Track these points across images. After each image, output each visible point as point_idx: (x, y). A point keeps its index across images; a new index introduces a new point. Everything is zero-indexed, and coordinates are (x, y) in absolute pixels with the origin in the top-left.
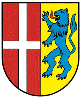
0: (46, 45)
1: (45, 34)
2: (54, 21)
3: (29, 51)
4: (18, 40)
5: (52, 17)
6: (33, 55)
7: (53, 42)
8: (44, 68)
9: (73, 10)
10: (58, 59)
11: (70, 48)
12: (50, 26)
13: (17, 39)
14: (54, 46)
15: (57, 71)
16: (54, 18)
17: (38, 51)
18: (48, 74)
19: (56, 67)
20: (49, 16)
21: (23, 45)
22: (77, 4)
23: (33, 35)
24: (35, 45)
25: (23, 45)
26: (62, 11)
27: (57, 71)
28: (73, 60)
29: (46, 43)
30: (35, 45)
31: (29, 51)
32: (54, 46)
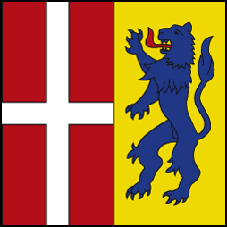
0: (137, 116)
1: (129, 78)
2: (156, 54)
3: (76, 132)
4: (71, 127)
5: (150, 43)
6: (91, 146)
7: (155, 107)
8: (126, 172)
9: (206, 22)
10: (166, 152)
11: (199, 125)
12: (146, 63)
13: (41, 96)
14: (156, 116)
15: (173, 181)
16: (157, 46)
17: (107, 132)
18: (141, 189)
19: (161, 172)
20: (143, 42)
21: (57, 113)
22: (112, 123)
23: (91, 80)
24: (95, 113)
25: (57, 113)
26: (176, 29)
27: (166, 181)
28: (208, 154)
29: (138, 109)
30: (95, 113)
31: (76, 132)
32: (156, 116)
